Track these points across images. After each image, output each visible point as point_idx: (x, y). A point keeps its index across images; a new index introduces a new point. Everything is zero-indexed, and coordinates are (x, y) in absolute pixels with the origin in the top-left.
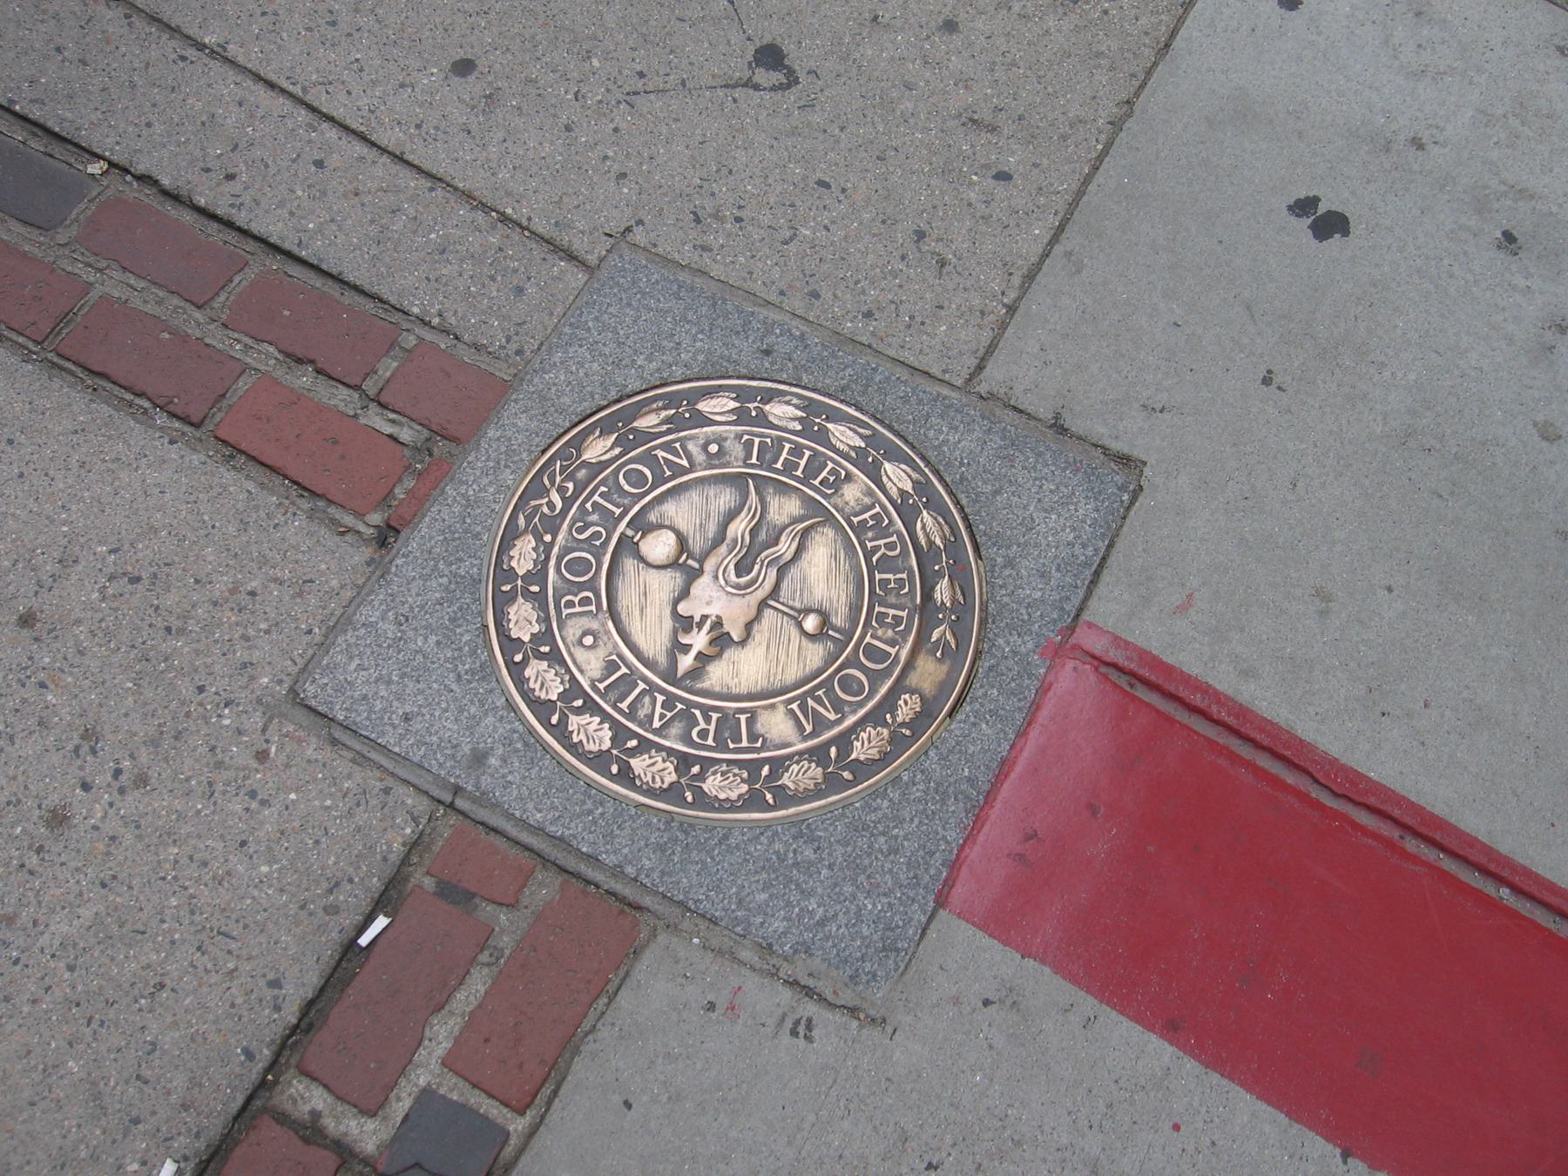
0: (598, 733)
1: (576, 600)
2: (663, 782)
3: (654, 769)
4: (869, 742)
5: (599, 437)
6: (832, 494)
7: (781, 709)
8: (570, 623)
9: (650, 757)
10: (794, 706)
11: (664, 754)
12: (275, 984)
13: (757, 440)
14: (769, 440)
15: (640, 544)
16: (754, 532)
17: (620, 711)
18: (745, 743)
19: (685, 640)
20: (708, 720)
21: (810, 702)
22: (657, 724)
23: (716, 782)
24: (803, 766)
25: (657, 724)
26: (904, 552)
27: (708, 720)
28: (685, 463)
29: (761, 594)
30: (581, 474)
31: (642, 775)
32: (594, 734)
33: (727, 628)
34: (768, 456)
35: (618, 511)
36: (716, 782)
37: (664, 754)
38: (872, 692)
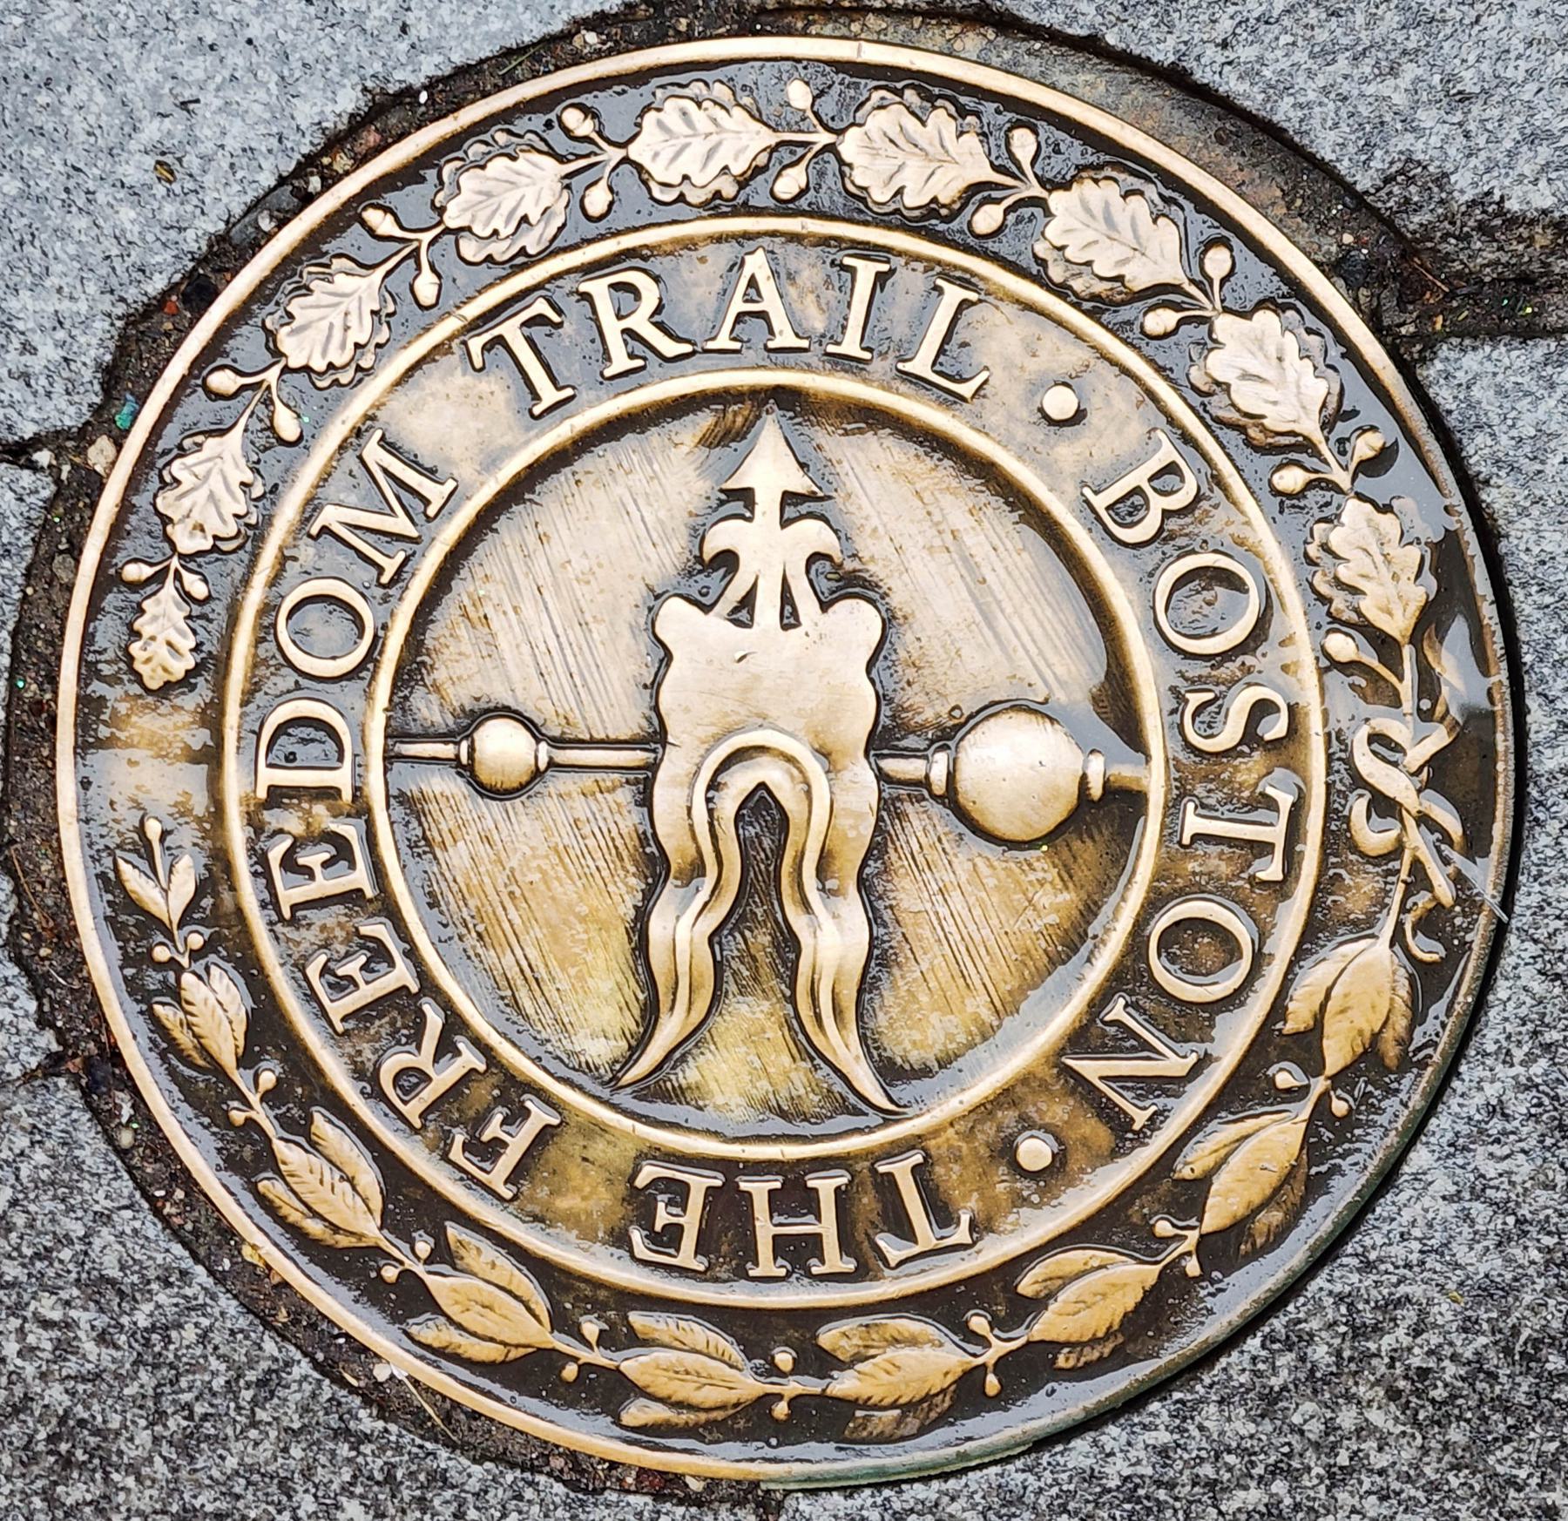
0: (891, 165)
1: (1158, 503)
2: (660, 124)
3: (699, 147)
4: (212, 497)
5: (1376, 1037)
6: (636, 1172)
7: (466, 472)
8: (1136, 429)
9: (725, 170)
10: (435, 493)
11: (695, 197)
12: (577, 482)
13: (926, 1234)
14: (893, 1255)
15: (1081, 757)
16: (788, 944)
17: (867, 250)
18: (510, 329)
19: (812, 535)
20: (445, 1048)
21: (401, 524)
22: (757, 264)
23: (530, 193)
24: (343, 346)
25: (757, 264)
26: (366, 1076)
27: (445, 1048)
28: (1091, 1069)
29: (673, 766)
30: (1359, 889)
31: (720, 114)
32: (901, 156)
33: (715, 625)
34: (868, 1201)
35: (1194, 824)
36: (530, 193)
37: (695, 197)
38: (265, 631)
